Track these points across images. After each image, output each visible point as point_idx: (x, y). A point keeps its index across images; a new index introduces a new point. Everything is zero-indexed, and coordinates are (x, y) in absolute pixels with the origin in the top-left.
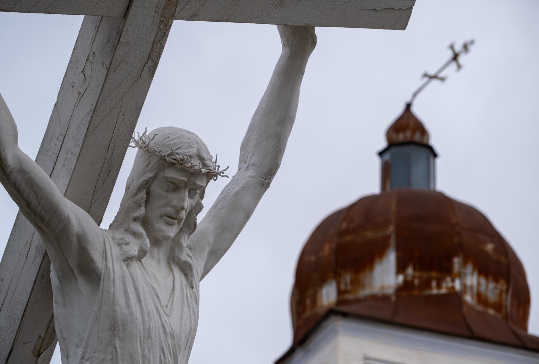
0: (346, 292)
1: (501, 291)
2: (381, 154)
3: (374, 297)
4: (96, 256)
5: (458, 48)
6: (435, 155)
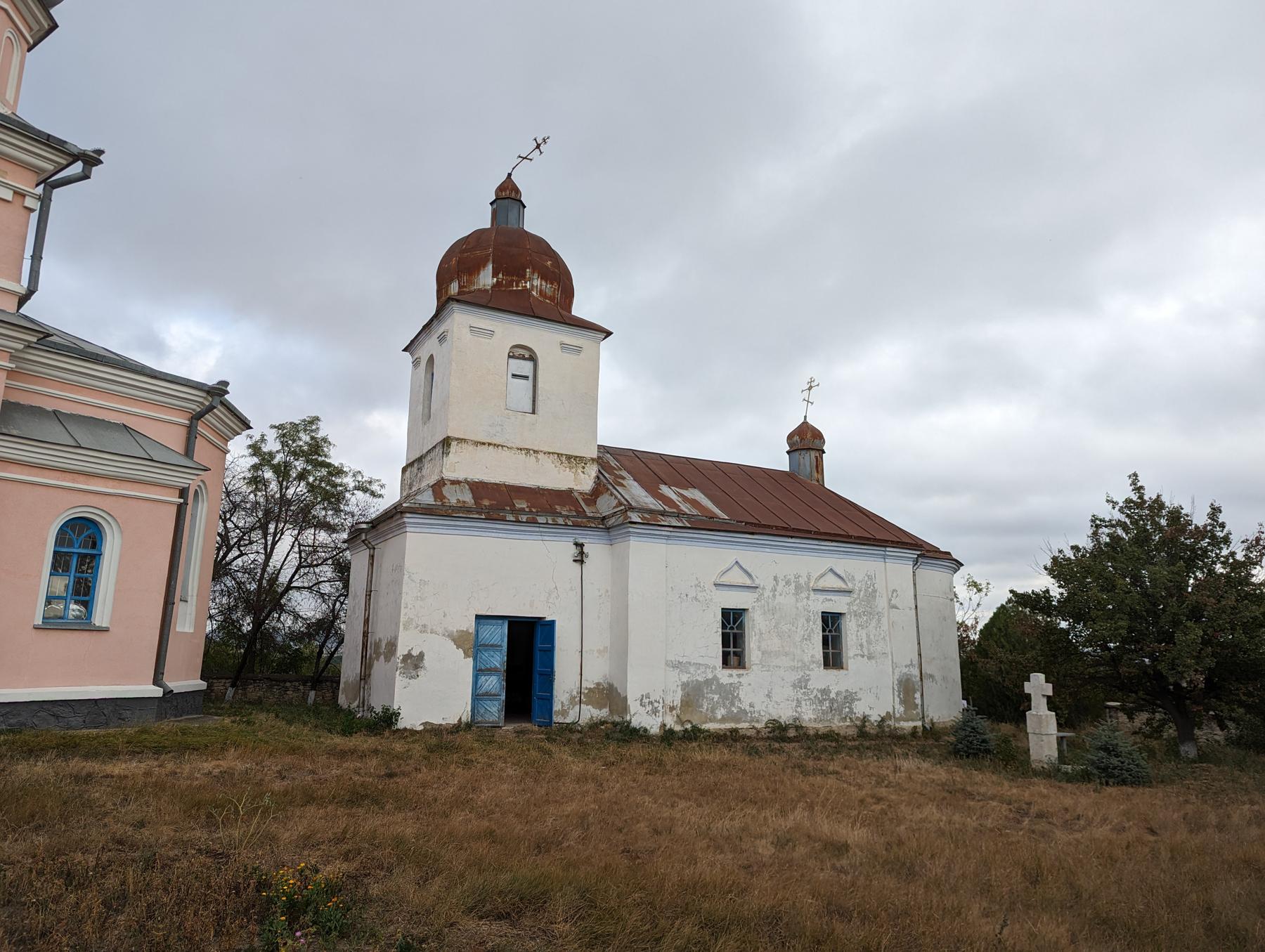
1: (555, 289)
5: (540, 141)
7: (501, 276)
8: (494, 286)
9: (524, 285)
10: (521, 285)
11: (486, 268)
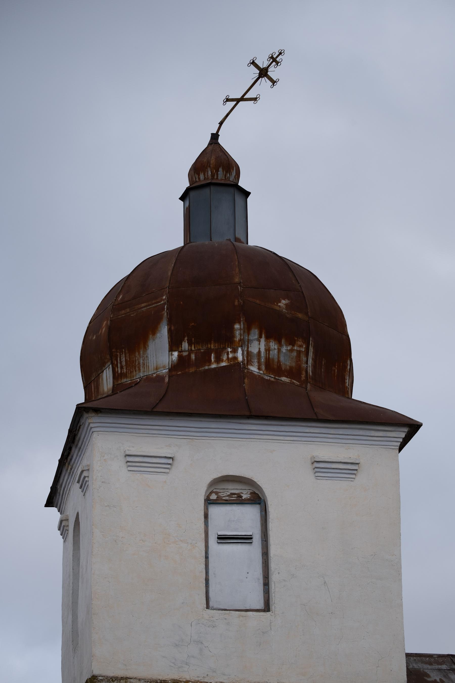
1: (299, 352)
3: (149, 379)
5: (263, 62)
7: (185, 345)
8: (173, 368)
9: (231, 356)
10: (225, 358)
11: (158, 335)
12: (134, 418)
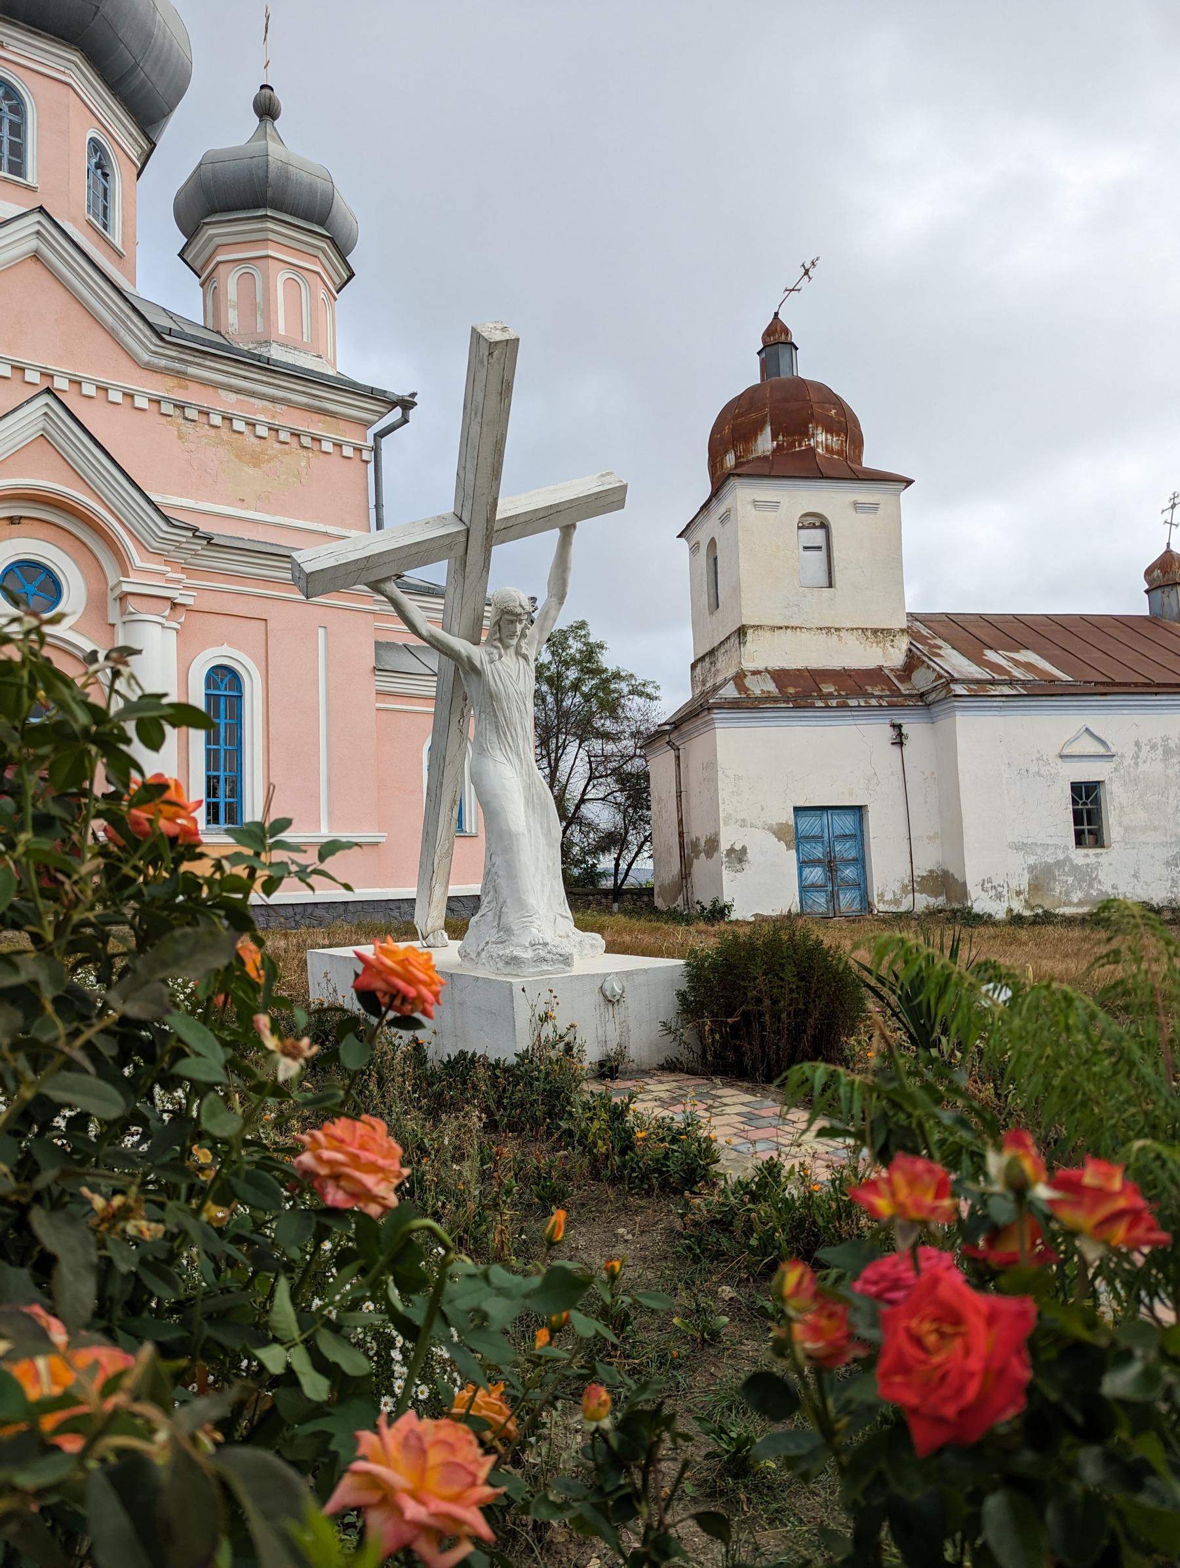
0: (741, 457)
2: (759, 353)
3: (758, 458)
4: (478, 664)
6: (796, 349)
7: (781, 438)
8: (774, 451)
12: (378, 506)
